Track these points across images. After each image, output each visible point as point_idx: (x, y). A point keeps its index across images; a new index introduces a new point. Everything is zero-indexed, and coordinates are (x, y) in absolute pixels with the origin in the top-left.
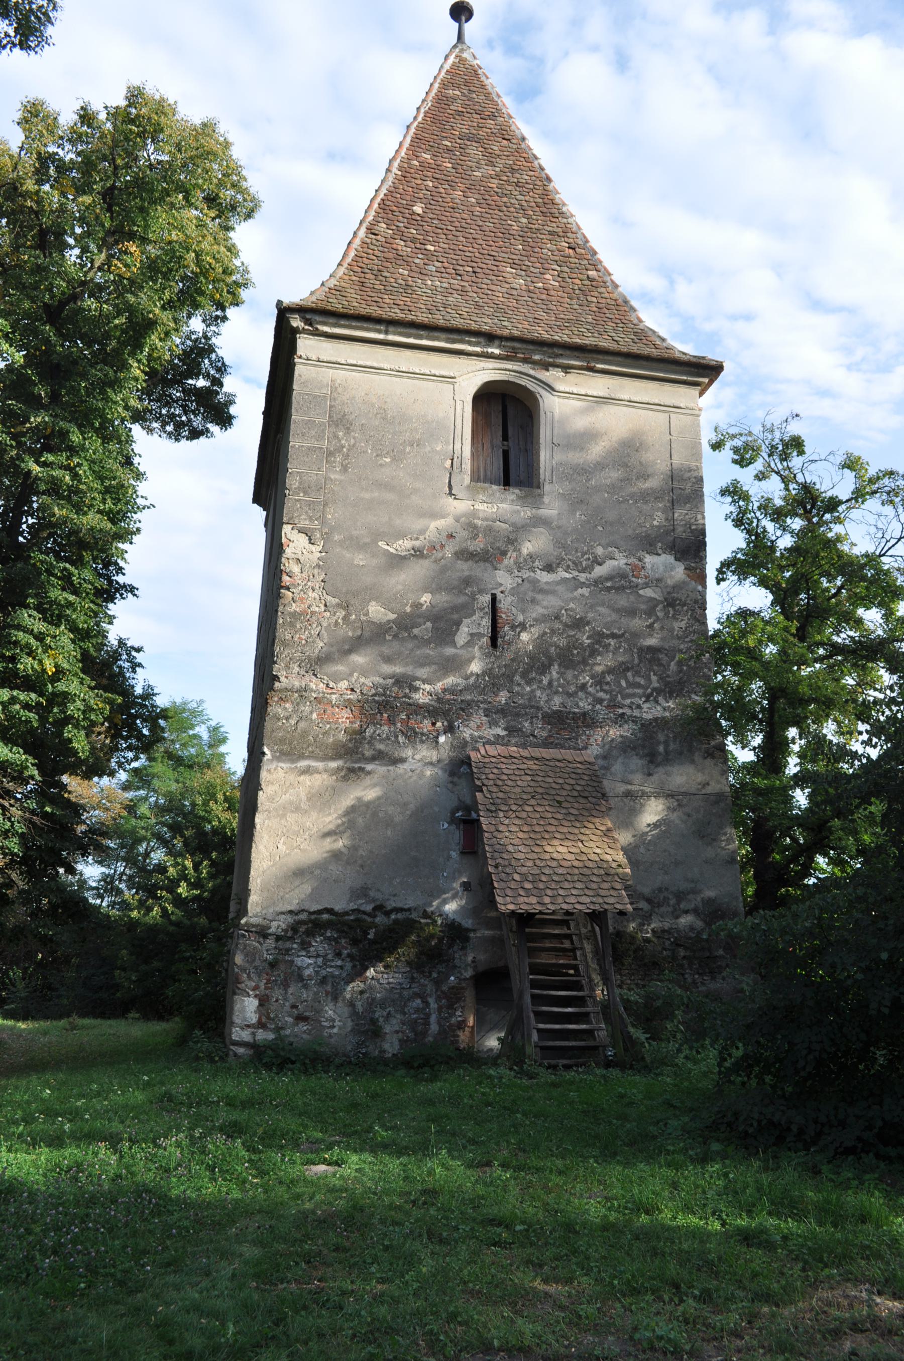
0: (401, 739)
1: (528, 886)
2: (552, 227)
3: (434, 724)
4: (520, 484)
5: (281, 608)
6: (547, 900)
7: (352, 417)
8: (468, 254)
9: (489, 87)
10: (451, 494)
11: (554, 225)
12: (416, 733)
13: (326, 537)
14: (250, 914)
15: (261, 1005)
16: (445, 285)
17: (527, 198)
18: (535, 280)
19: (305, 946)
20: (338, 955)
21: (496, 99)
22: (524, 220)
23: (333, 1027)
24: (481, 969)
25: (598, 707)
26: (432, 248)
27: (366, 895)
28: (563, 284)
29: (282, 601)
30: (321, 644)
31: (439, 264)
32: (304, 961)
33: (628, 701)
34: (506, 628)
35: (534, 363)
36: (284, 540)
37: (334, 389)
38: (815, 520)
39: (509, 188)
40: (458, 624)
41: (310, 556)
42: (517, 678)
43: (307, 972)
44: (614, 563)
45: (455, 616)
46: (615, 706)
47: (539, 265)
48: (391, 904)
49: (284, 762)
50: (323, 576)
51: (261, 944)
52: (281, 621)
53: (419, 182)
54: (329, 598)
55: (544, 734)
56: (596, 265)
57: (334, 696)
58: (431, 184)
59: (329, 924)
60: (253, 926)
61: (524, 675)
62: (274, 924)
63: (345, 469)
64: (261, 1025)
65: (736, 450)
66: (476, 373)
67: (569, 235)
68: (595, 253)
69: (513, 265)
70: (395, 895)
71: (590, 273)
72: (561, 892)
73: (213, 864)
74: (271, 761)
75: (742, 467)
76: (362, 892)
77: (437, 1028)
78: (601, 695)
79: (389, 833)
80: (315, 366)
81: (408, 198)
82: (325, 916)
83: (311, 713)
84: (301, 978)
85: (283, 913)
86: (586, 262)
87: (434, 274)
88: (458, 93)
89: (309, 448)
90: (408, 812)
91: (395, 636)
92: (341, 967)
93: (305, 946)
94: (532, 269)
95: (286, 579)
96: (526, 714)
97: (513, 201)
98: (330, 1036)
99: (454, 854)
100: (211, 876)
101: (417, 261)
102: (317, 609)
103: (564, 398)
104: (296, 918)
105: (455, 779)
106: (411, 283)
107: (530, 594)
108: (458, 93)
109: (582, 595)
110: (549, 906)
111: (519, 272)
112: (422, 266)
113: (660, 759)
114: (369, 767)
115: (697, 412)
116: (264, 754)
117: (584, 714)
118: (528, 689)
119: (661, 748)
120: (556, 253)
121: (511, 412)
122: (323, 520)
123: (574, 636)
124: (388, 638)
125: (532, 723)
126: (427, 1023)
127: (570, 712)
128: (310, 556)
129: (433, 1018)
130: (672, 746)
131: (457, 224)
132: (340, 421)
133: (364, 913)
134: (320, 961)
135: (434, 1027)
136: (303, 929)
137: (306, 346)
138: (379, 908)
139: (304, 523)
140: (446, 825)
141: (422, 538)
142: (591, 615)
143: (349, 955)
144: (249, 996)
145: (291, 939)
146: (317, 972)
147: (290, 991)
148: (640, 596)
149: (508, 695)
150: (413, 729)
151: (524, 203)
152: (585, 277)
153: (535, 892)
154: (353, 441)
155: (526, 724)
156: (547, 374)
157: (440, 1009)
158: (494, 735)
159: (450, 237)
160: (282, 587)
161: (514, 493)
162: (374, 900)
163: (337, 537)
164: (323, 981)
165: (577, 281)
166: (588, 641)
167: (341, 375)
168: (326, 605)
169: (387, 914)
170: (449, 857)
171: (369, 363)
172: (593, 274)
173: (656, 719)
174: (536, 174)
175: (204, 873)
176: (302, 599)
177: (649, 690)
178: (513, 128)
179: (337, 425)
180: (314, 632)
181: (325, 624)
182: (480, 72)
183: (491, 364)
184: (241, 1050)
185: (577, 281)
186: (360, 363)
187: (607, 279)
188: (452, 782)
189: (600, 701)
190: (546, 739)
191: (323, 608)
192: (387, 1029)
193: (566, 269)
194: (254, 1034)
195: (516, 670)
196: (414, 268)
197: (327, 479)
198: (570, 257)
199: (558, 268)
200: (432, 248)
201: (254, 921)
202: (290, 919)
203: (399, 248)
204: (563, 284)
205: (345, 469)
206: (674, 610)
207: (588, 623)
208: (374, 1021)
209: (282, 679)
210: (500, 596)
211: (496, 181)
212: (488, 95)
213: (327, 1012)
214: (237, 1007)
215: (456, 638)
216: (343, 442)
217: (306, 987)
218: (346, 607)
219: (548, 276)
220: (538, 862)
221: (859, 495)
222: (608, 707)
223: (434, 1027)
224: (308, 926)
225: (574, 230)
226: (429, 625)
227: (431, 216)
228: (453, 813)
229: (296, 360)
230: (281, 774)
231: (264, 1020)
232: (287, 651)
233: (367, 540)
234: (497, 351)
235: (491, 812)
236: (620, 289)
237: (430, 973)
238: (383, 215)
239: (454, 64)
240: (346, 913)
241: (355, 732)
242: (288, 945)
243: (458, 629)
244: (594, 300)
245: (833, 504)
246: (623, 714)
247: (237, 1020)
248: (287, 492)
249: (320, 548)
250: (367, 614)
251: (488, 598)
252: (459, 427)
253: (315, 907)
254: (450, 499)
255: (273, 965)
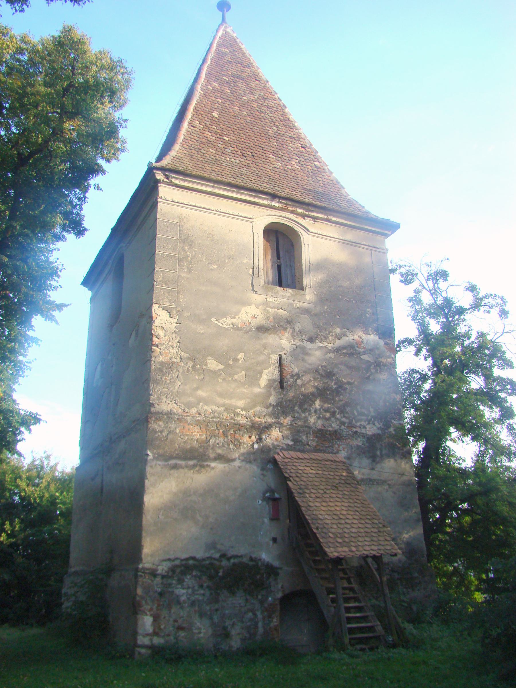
0: (231, 446)
1: (340, 540)
2: (291, 134)
3: (250, 437)
4: (288, 286)
5: (153, 359)
6: (354, 549)
7: (193, 238)
8: (247, 144)
9: (244, 50)
10: (253, 290)
11: (291, 133)
12: (240, 443)
13: (180, 314)
14: (144, 561)
15: (155, 620)
16: (238, 161)
17: (275, 116)
18: (287, 164)
19: (180, 581)
20: (201, 586)
21: (249, 57)
22: (275, 128)
23: (200, 633)
24: (287, 592)
25: (343, 427)
26: (227, 139)
27: (215, 548)
28: (302, 168)
29: (154, 354)
30: (179, 383)
31: (232, 149)
32: (181, 592)
33: (358, 424)
34: (288, 377)
35: (298, 214)
36: (154, 314)
37: (181, 220)
38: (450, 319)
39: (264, 108)
40: (261, 373)
41: (170, 326)
42: (296, 408)
43: (183, 598)
44: (347, 338)
45: (259, 368)
46: (352, 427)
47: (287, 156)
48: (231, 553)
49: (160, 460)
50: (178, 339)
51: (152, 581)
52: (153, 367)
53: (214, 99)
54: (183, 353)
55: (314, 444)
56: (318, 159)
57: (188, 418)
58: (220, 101)
59: (194, 567)
60: (147, 569)
61: (300, 407)
62: (160, 568)
63: (190, 271)
64: (155, 633)
65: (402, 275)
66: (264, 217)
67: (301, 140)
68: (317, 152)
69: (273, 154)
70: (232, 547)
71: (316, 163)
72: (359, 544)
73: (22, 521)
74: (153, 460)
75: (405, 284)
76: (212, 546)
77: (263, 631)
78: (344, 419)
79: (227, 507)
80: (170, 204)
81: (209, 107)
82: (191, 562)
83: (176, 428)
84: (179, 602)
85: (165, 560)
86: (312, 157)
87: (230, 154)
88: (227, 50)
89: (168, 256)
90: (238, 494)
91: (224, 380)
92: (203, 595)
93: (180, 581)
94: (284, 157)
95: (155, 339)
96: (304, 431)
97: (267, 116)
98: (199, 638)
99: (266, 520)
100: (22, 530)
101: (219, 145)
102: (175, 360)
103: (314, 236)
104: (173, 563)
105: (265, 472)
106: (218, 158)
107: (301, 355)
108: (227, 50)
109: (330, 358)
110: (357, 552)
111: (277, 158)
112: (222, 148)
113: (378, 459)
114: (213, 464)
115: (385, 251)
116: (148, 455)
117: (336, 431)
118: (303, 415)
119: (378, 453)
120: (295, 149)
121: (281, 242)
122: (177, 302)
123: (327, 382)
124: (220, 380)
125: (307, 437)
126: (256, 627)
127: (327, 430)
128: (170, 326)
129: (260, 624)
130: (384, 452)
131: (238, 126)
132: (185, 240)
133: (214, 559)
134: (190, 591)
135: (261, 630)
136: (178, 570)
137: (164, 191)
138: (223, 556)
139: (166, 304)
140: (260, 502)
141: (237, 317)
142: (336, 370)
143: (208, 587)
144: (147, 615)
145: (171, 577)
146: (189, 598)
147: (173, 611)
148: (361, 359)
149: (292, 419)
150: (237, 440)
151: (273, 118)
152: (313, 166)
153: (345, 544)
154: (194, 253)
155: (304, 437)
156: (304, 221)
157: (264, 618)
158: (286, 444)
159: (236, 133)
160: (153, 345)
161: (289, 292)
162: (219, 551)
163: (186, 314)
164: (193, 604)
165: (309, 167)
166: (335, 386)
167: (185, 211)
168: (181, 358)
169: (229, 559)
170: (263, 522)
171: (202, 206)
172: (317, 163)
173: (374, 435)
174: (277, 102)
175: (17, 528)
176: (166, 354)
177: (370, 417)
178: (260, 74)
179: (184, 243)
180: (175, 376)
181: (181, 370)
182: (237, 40)
183: (273, 212)
184: (143, 651)
185: (309, 167)
186: (197, 205)
187: (325, 168)
188: (263, 474)
189: (343, 423)
190: (315, 447)
191: (179, 360)
192: (233, 632)
193: (302, 159)
194: (151, 640)
195: (296, 403)
196: (218, 149)
197: (179, 276)
198: (303, 153)
199: (298, 159)
200: (227, 139)
201: (147, 565)
202: (169, 564)
203: (209, 137)
204: (302, 168)
205: (190, 271)
206: (380, 369)
207: (334, 375)
208: (225, 628)
209: (156, 406)
210: (284, 356)
211: (256, 104)
212: (244, 54)
213: (196, 624)
214: (140, 622)
215: (261, 382)
216: (188, 253)
217: (182, 608)
218: (194, 359)
219: (293, 163)
220: (339, 525)
221: (476, 306)
222: (348, 427)
223: (261, 630)
224: (183, 568)
225: (303, 137)
226: (244, 373)
227: (223, 119)
228: (264, 494)
229: (158, 200)
230: (159, 469)
231: (157, 630)
232: (159, 387)
233: (204, 317)
234: (277, 205)
235: (301, 494)
236: (333, 175)
237: (257, 596)
238: (196, 116)
239: (223, 34)
240: (204, 560)
241: (202, 442)
242: (170, 581)
243: (261, 376)
244: (320, 179)
245: (461, 311)
246: (356, 432)
247: (140, 631)
248: (155, 283)
249: (176, 321)
250: (206, 365)
251: (277, 357)
252: (256, 249)
253: (184, 556)
254: (253, 294)
255: (161, 594)
